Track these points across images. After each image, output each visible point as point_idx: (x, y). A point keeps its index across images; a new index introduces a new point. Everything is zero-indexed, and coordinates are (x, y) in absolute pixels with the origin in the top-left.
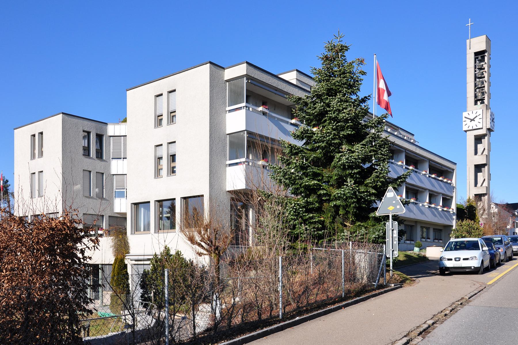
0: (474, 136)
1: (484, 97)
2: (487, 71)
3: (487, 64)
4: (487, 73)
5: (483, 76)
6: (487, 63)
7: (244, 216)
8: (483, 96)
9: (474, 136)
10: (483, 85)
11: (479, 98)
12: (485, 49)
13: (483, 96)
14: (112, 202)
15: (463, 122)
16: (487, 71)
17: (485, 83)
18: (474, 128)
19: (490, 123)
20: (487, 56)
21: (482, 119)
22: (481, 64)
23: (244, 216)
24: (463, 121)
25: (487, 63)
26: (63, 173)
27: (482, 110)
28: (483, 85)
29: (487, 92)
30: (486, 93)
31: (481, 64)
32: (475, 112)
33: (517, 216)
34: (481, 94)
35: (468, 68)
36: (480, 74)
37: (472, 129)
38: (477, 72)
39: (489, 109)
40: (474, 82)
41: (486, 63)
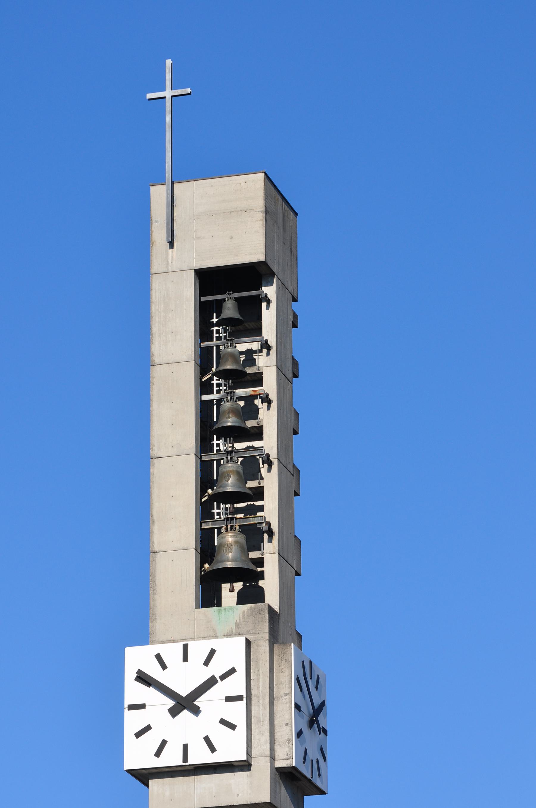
18: (192, 760)
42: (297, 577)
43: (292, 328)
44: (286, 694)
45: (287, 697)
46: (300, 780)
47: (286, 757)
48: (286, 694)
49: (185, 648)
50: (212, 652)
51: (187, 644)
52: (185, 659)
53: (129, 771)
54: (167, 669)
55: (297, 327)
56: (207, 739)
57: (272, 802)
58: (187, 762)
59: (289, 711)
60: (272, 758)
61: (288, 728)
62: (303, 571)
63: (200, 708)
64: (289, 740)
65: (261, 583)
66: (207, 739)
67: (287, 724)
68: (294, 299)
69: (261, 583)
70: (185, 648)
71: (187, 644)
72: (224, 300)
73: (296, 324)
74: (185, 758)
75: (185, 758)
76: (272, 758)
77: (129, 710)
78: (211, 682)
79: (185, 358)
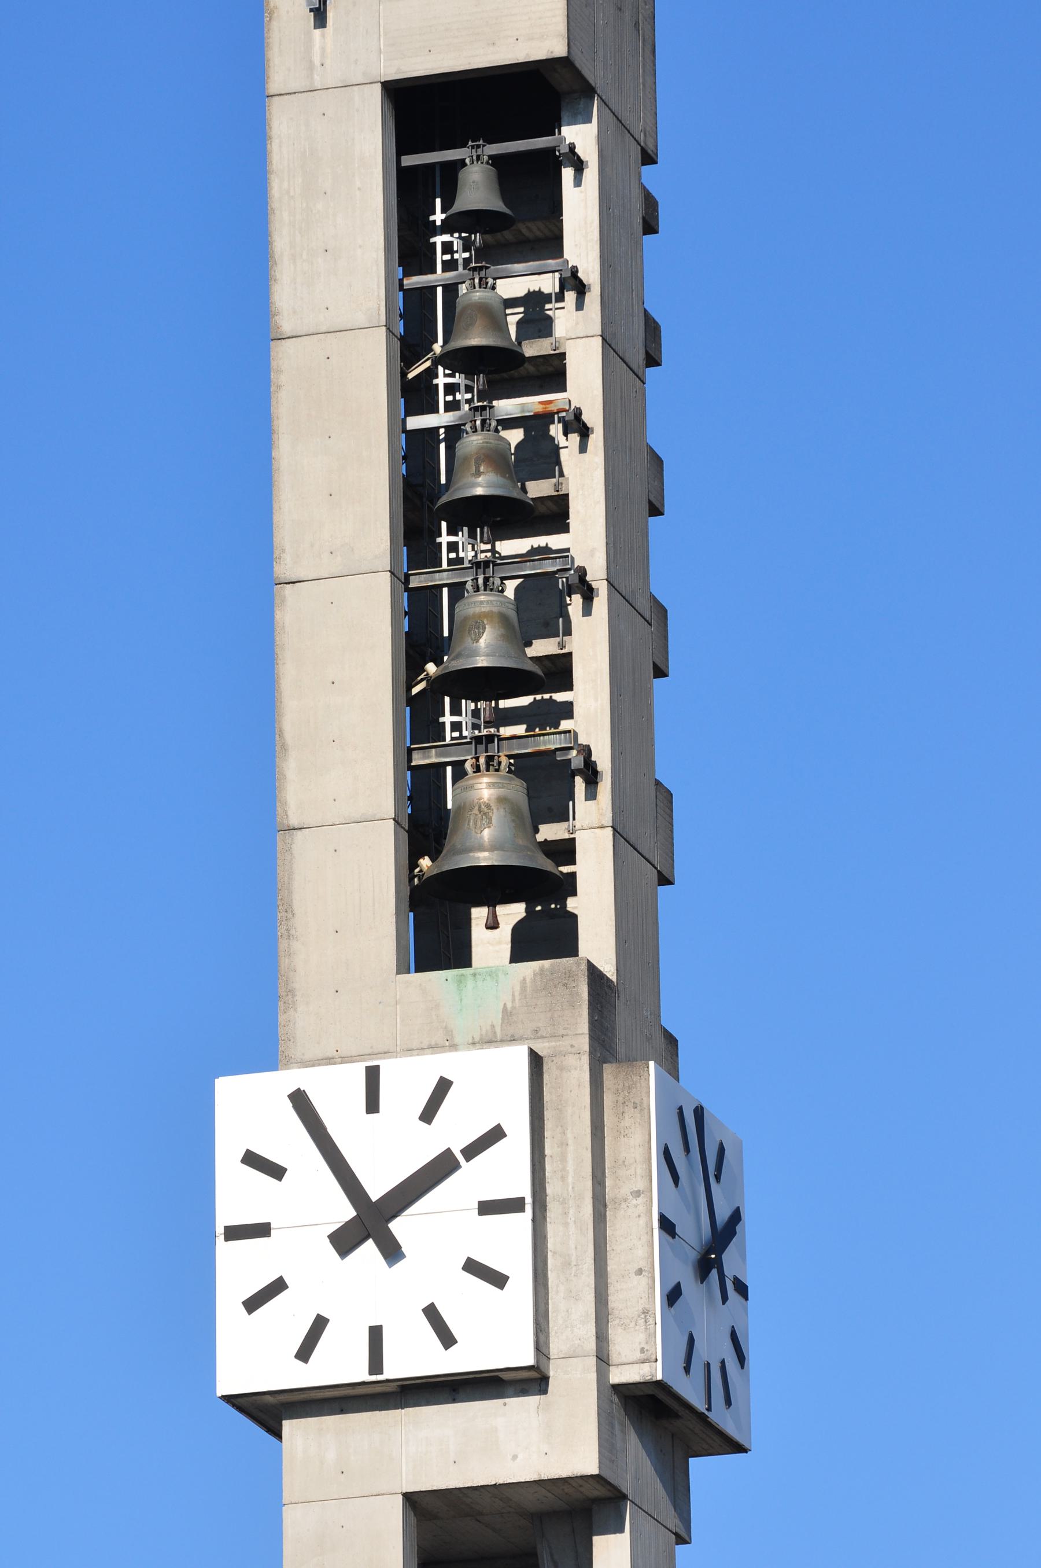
0: (412, 1501)
1: (565, 851)
2: (594, 417)
3: (593, 298)
4: (596, 439)
5: (538, 489)
6: (590, 272)
7: (517, 998)
8: (549, 832)
9: (412, 1501)
10: (543, 647)
11: (484, 858)
12: (558, 48)
13: (549, 832)
14: (598, 973)
15: (226, 1251)
16: (594, 417)
17: (568, 445)
18: (395, 1368)
19: (673, 1296)
20: (591, 174)
21: (523, 1221)
22: (511, 287)
23: (517, 998)
24: (226, 1216)
25: (590, 272)
26: (617, 964)
27: (518, 1057)
28: (543, 647)
29: (603, 759)
30: (591, 775)
31: (511, 287)
33: (404, 375)
34: (517, 789)
35: (286, 324)
36: (496, 458)
37: (358, 1372)
38: (439, 419)
39: (634, 1059)
40: (401, 580)
41: (572, 282)
44: (637, 1194)
45: (641, 1200)
47: (638, 1355)
48: (637, 1194)
49: (373, 1075)
59: (645, 1238)
60: (603, 1360)
61: (643, 1281)
64: (645, 1312)
67: (640, 1272)
70: (373, 1075)
72: (462, 163)
74: (376, 1363)
76: (603, 1360)
79: (361, 319)
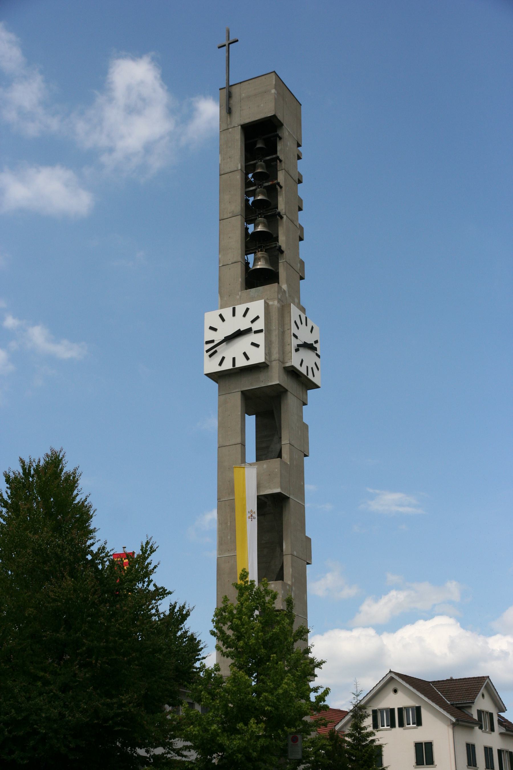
32: (240, 309)
42: (301, 281)
43: (298, 210)
46: (301, 377)
49: (234, 309)
50: (247, 309)
51: (235, 307)
52: (234, 315)
53: (207, 375)
54: (222, 315)
55: (302, 210)
56: (245, 354)
57: (283, 384)
58: (235, 366)
62: (304, 208)
63: (240, 330)
65: (310, 655)
66: (245, 354)
68: (299, 145)
69: (310, 655)
70: (234, 309)
71: (235, 307)
73: (301, 180)
74: (234, 364)
75: (234, 364)
77: (206, 344)
78: (248, 331)
